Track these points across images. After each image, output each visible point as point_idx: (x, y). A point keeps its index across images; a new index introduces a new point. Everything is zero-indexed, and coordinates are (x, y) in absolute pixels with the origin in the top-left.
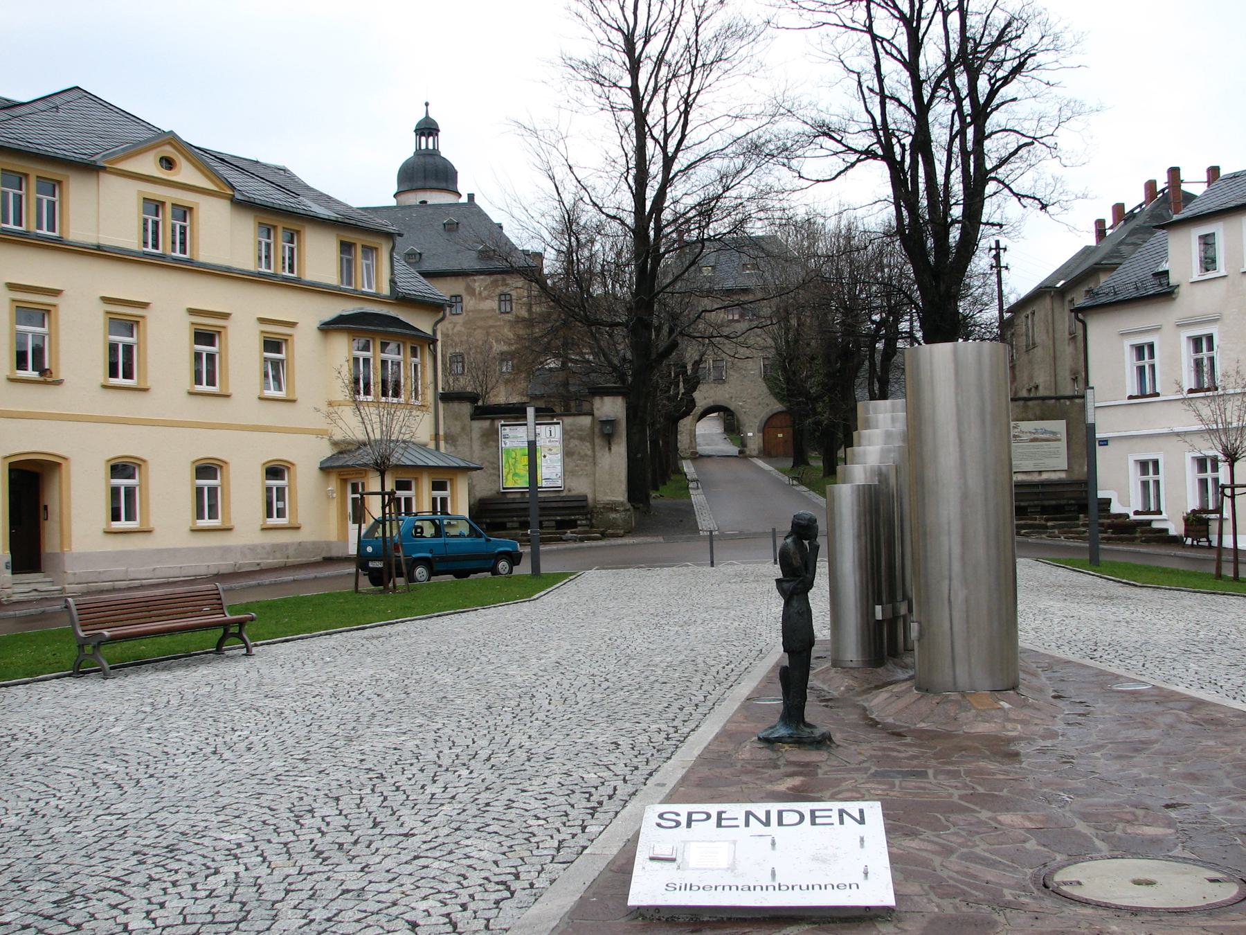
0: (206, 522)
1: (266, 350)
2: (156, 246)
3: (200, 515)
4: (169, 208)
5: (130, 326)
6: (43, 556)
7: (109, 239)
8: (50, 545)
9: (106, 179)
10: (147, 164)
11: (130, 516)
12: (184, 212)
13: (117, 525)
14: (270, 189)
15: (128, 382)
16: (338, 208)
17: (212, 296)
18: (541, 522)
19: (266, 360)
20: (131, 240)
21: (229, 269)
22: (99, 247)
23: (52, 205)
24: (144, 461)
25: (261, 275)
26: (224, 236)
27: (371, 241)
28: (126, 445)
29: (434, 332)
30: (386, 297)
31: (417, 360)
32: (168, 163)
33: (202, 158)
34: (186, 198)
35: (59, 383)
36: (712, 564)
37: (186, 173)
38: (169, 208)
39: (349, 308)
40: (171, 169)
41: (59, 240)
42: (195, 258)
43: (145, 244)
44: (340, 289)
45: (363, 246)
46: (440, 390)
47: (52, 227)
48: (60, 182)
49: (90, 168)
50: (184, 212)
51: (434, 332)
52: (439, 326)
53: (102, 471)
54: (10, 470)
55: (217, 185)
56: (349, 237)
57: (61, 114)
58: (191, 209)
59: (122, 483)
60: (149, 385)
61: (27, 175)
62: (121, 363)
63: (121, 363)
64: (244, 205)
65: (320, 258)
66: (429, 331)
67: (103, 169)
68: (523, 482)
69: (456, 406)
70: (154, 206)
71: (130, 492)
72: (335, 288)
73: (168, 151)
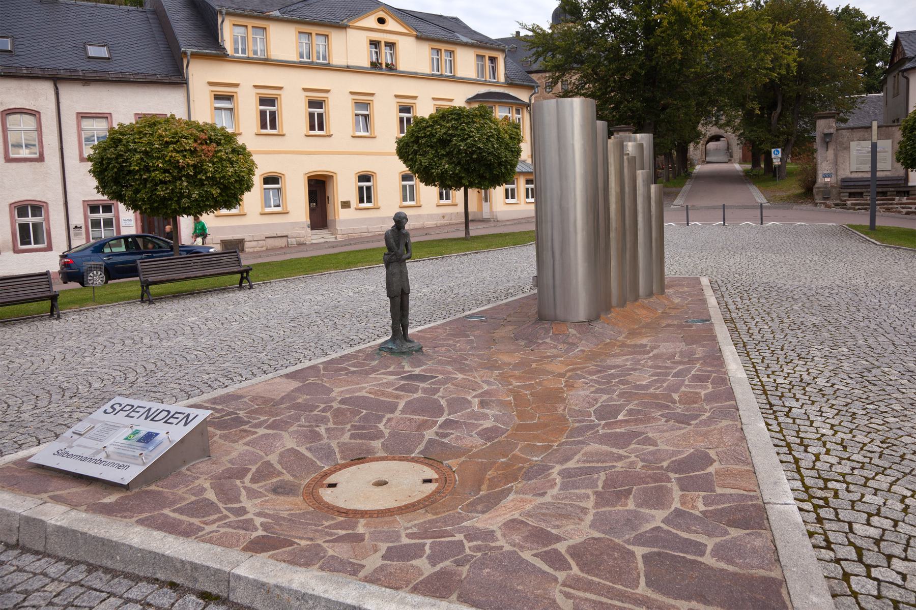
0: (444, 202)
2: (244, 51)
3: (405, 199)
4: (383, 44)
5: (366, 105)
7: (353, 62)
8: (330, 217)
9: (348, 30)
11: (369, 201)
12: (391, 45)
13: (442, 202)
14: (438, 30)
15: (321, 133)
16: (477, 37)
19: (357, 115)
21: (416, 73)
22: (348, 67)
25: (433, 75)
28: (365, 166)
29: (530, 100)
31: (520, 116)
39: (483, 90)
41: (328, 64)
43: (302, 57)
51: (530, 100)
53: (354, 179)
56: (482, 52)
59: (365, 184)
60: (284, 132)
62: (317, 123)
63: (317, 123)
67: (349, 27)
68: (469, 190)
70: (375, 44)
73: (381, 14)
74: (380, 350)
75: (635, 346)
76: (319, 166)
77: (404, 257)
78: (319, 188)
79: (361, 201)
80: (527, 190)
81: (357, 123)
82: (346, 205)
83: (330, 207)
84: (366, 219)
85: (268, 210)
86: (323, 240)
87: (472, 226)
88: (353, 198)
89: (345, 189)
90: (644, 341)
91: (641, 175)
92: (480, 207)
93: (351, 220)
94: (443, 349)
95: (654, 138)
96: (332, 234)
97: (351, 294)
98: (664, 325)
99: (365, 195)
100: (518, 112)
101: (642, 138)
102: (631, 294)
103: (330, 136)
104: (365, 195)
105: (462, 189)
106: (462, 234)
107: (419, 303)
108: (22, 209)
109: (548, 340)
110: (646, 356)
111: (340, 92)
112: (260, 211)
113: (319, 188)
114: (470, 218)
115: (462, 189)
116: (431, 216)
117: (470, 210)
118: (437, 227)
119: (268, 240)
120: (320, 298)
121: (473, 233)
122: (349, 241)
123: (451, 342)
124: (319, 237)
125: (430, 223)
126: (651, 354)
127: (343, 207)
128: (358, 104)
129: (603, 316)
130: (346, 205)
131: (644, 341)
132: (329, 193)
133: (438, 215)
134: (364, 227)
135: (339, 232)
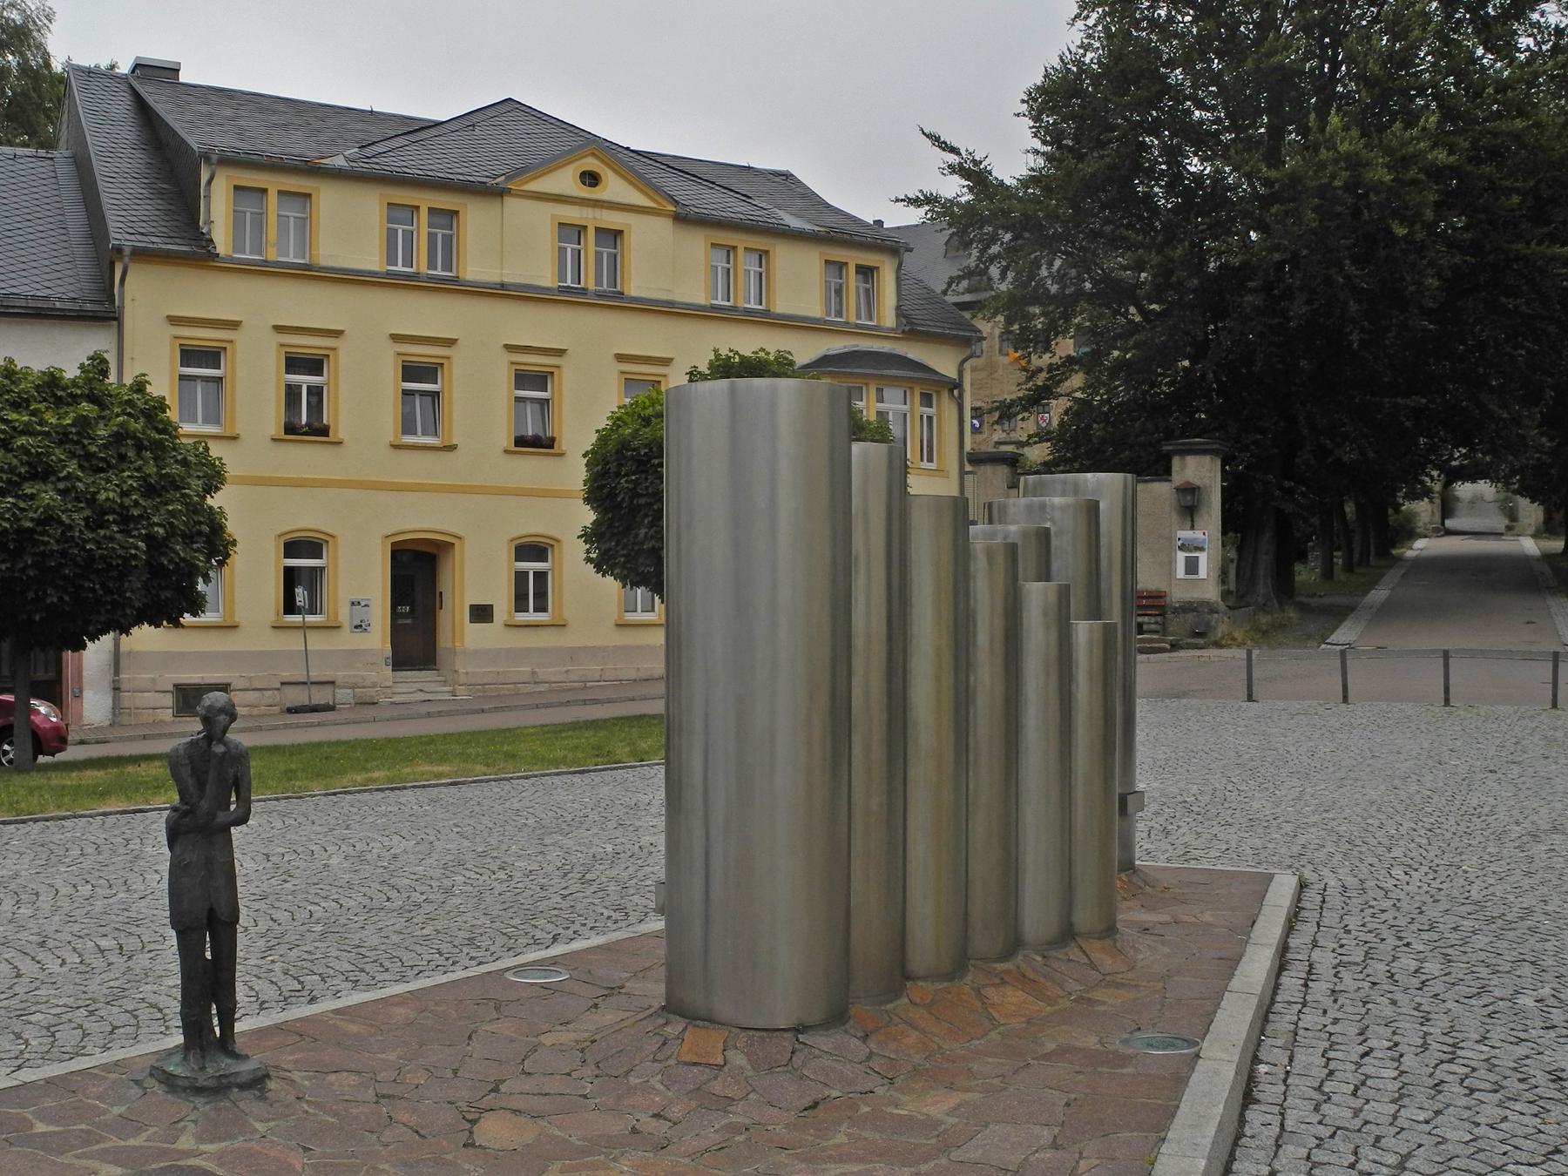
1: (517, 388)
5: (539, 380)
6: (439, 652)
10: (565, 181)
11: (541, 607)
12: (613, 236)
17: (647, 336)
18: (1140, 625)
19: (518, 399)
20: (373, 261)
21: (671, 304)
22: (503, 286)
23: (448, 240)
24: (558, 541)
25: (714, 308)
26: (663, 260)
27: (868, 259)
28: (306, 518)
30: (892, 330)
32: (591, 179)
33: (643, 167)
34: (612, 219)
35: (562, 455)
36: (1250, 698)
37: (615, 187)
38: (591, 233)
39: (838, 345)
40: (595, 185)
42: (315, 261)
44: (826, 322)
45: (280, 192)
46: (968, 448)
47: (448, 266)
48: (767, 252)
49: (492, 192)
50: (613, 236)
52: (967, 365)
53: (505, 554)
54: (394, 553)
55: (653, 200)
56: (838, 254)
57: (477, 132)
58: (621, 232)
59: (532, 566)
61: (735, 248)
64: (684, 219)
65: (799, 282)
66: (952, 373)
69: (988, 470)
71: (541, 577)
72: (817, 321)
73: (591, 164)
76: (420, 519)
78: (417, 570)
79: (520, 603)
82: (482, 613)
88: (502, 601)
98: (1051, 1046)
108: (293, 547)
111: (480, 345)
113: (417, 570)
130: (482, 613)
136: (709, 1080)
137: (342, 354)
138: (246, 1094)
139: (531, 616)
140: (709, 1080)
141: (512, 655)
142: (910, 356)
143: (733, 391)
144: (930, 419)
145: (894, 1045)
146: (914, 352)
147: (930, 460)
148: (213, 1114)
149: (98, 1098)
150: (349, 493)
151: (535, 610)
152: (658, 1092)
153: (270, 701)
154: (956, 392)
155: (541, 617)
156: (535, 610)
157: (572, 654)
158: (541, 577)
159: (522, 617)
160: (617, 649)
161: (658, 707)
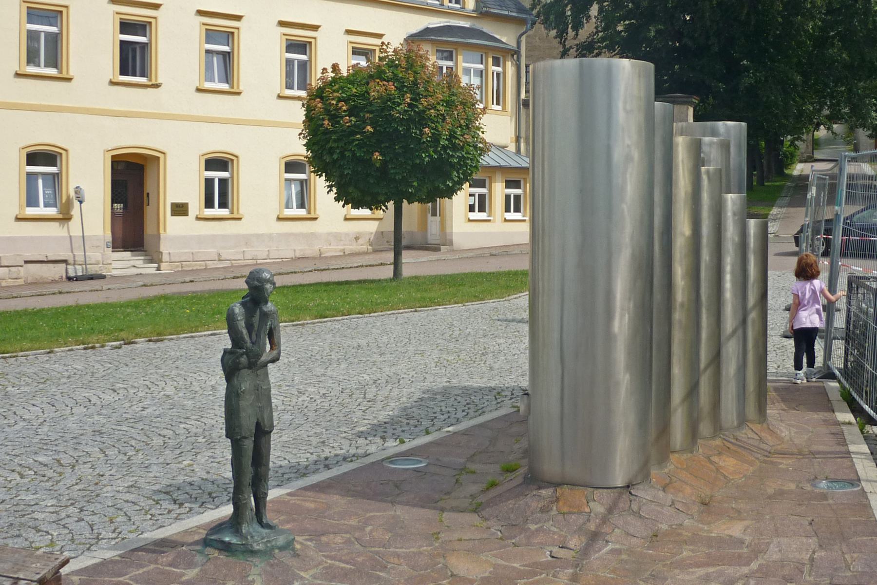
5: (229, 37)
8: (149, 230)
11: (223, 205)
19: (208, 52)
28: (218, 142)
29: (519, 43)
31: (499, 69)
51: (519, 43)
52: (523, 38)
59: (217, 175)
62: (133, 60)
63: (133, 60)
66: (513, 44)
74: (206, 543)
75: (721, 542)
77: (264, 358)
78: (132, 176)
79: (209, 204)
80: (508, 197)
81: (209, 67)
82: (180, 209)
83: (149, 211)
84: (214, 238)
85: (31, 211)
86: (135, 271)
87: (407, 257)
88: (195, 199)
89: (180, 180)
90: (736, 530)
91: (732, 200)
92: (423, 225)
93: (186, 237)
94: (339, 539)
95: (750, 136)
96: (152, 261)
97: (170, 391)
98: (770, 491)
99: (218, 194)
100: (496, 62)
101: (728, 129)
102: (704, 420)
103: (157, 86)
104: (218, 194)
105: (391, 205)
106: (388, 272)
107: (300, 420)
109: (548, 525)
110: (745, 570)
112: (16, 212)
113: (132, 176)
114: (404, 242)
115: (391, 205)
116: (337, 237)
117: (405, 228)
118: (345, 255)
119: (29, 265)
120: (109, 397)
121: (407, 271)
122: (187, 274)
123: (354, 522)
124: (125, 263)
125: (332, 249)
126: (754, 566)
127: (174, 213)
128: (211, 35)
129: (654, 472)
130: (180, 209)
131: (736, 530)
132: (149, 187)
133: (347, 234)
134: (210, 251)
135: (165, 258)
136: (585, 523)
137: (160, 20)
138: (284, 553)
139: (217, 212)
140: (585, 523)
141: (201, 240)
142: (485, 30)
143: (581, 61)
144: (498, 74)
145: (681, 494)
146: (487, 27)
147: (498, 104)
148: (268, 568)
149: (170, 565)
150: (79, 117)
151: (219, 207)
152: (554, 533)
153: (15, 276)
154: (515, 56)
155: (224, 212)
156: (219, 207)
157: (247, 239)
158: (223, 182)
159: (209, 212)
160: (280, 235)
161: (524, 264)
